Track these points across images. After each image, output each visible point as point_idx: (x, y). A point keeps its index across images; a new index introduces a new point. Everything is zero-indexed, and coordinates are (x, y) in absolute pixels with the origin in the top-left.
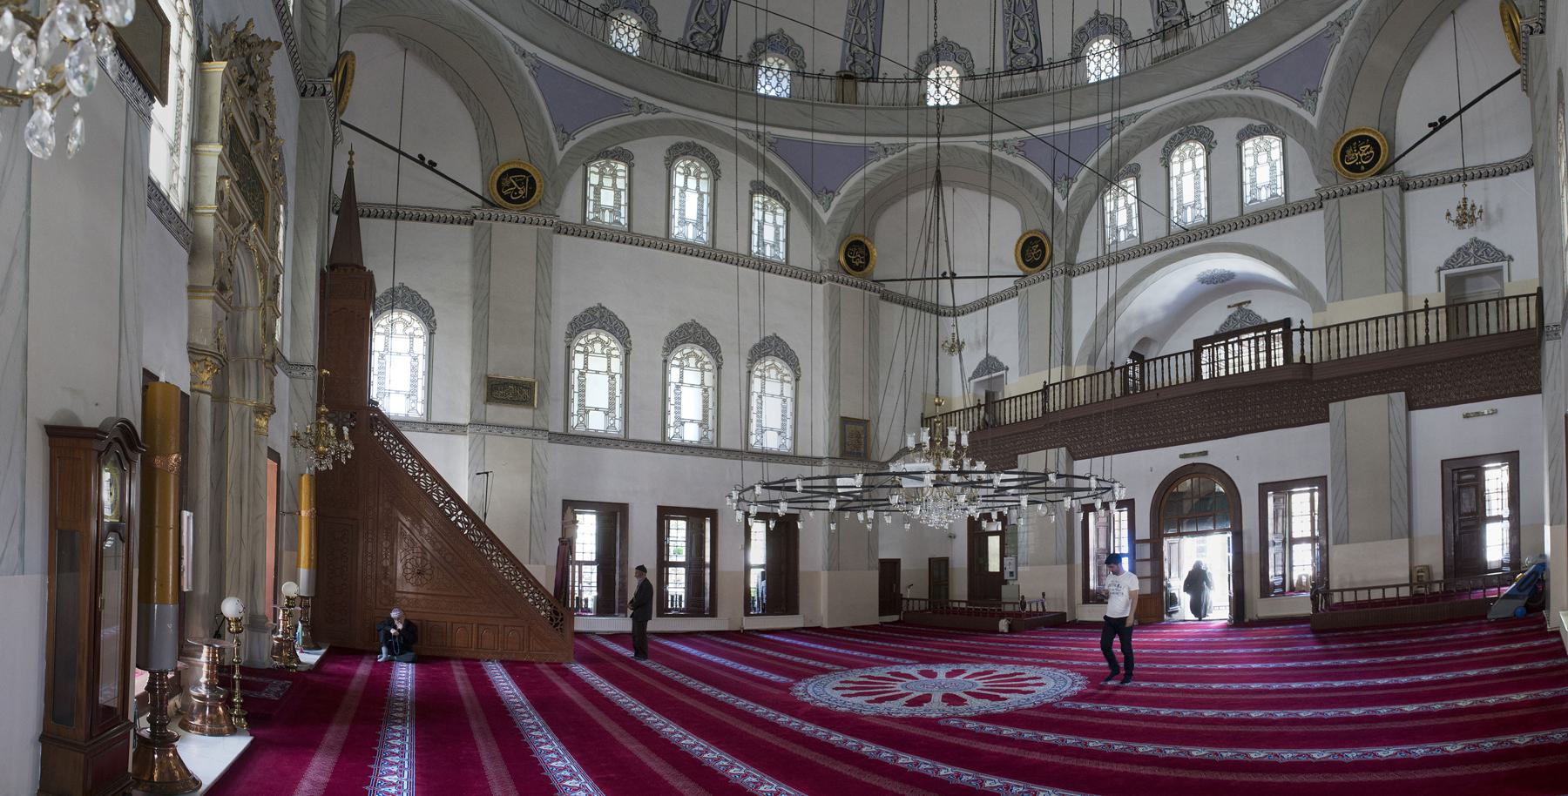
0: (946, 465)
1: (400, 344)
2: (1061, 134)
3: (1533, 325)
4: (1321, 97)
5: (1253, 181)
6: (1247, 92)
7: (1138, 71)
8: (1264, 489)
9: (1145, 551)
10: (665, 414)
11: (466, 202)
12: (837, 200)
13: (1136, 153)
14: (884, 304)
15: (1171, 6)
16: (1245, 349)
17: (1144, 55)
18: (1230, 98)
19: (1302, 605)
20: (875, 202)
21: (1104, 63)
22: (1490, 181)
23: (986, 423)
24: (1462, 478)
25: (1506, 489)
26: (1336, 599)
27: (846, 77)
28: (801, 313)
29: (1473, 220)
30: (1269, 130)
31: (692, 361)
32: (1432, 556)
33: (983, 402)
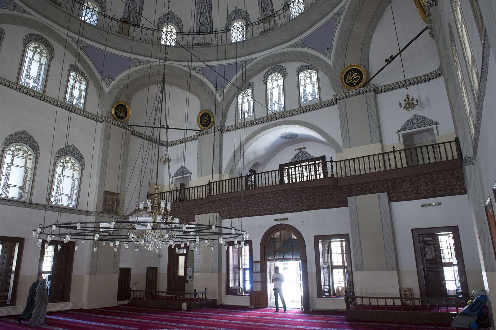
0: (159, 219)
1: (68, 172)
2: (221, 66)
3: (456, 157)
4: (333, 51)
5: (305, 91)
6: (300, 49)
7: (253, 38)
8: (317, 239)
9: (258, 267)
10: (51, 189)
11: (194, 133)
12: (114, 83)
13: (252, 77)
14: (132, 137)
15: (267, 7)
16: (304, 170)
17: (256, 30)
18: (292, 52)
19: (340, 304)
20: (133, 86)
21: (239, 33)
22: (420, 85)
23: (180, 199)
24: (425, 240)
25: (452, 247)
26: (359, 302)
27: (125, 21)
28: (89, 137)
29: (413, 106)
30: (310, 67)
31: (21, 153)
32: (412, 282)
33: (179, 188)
